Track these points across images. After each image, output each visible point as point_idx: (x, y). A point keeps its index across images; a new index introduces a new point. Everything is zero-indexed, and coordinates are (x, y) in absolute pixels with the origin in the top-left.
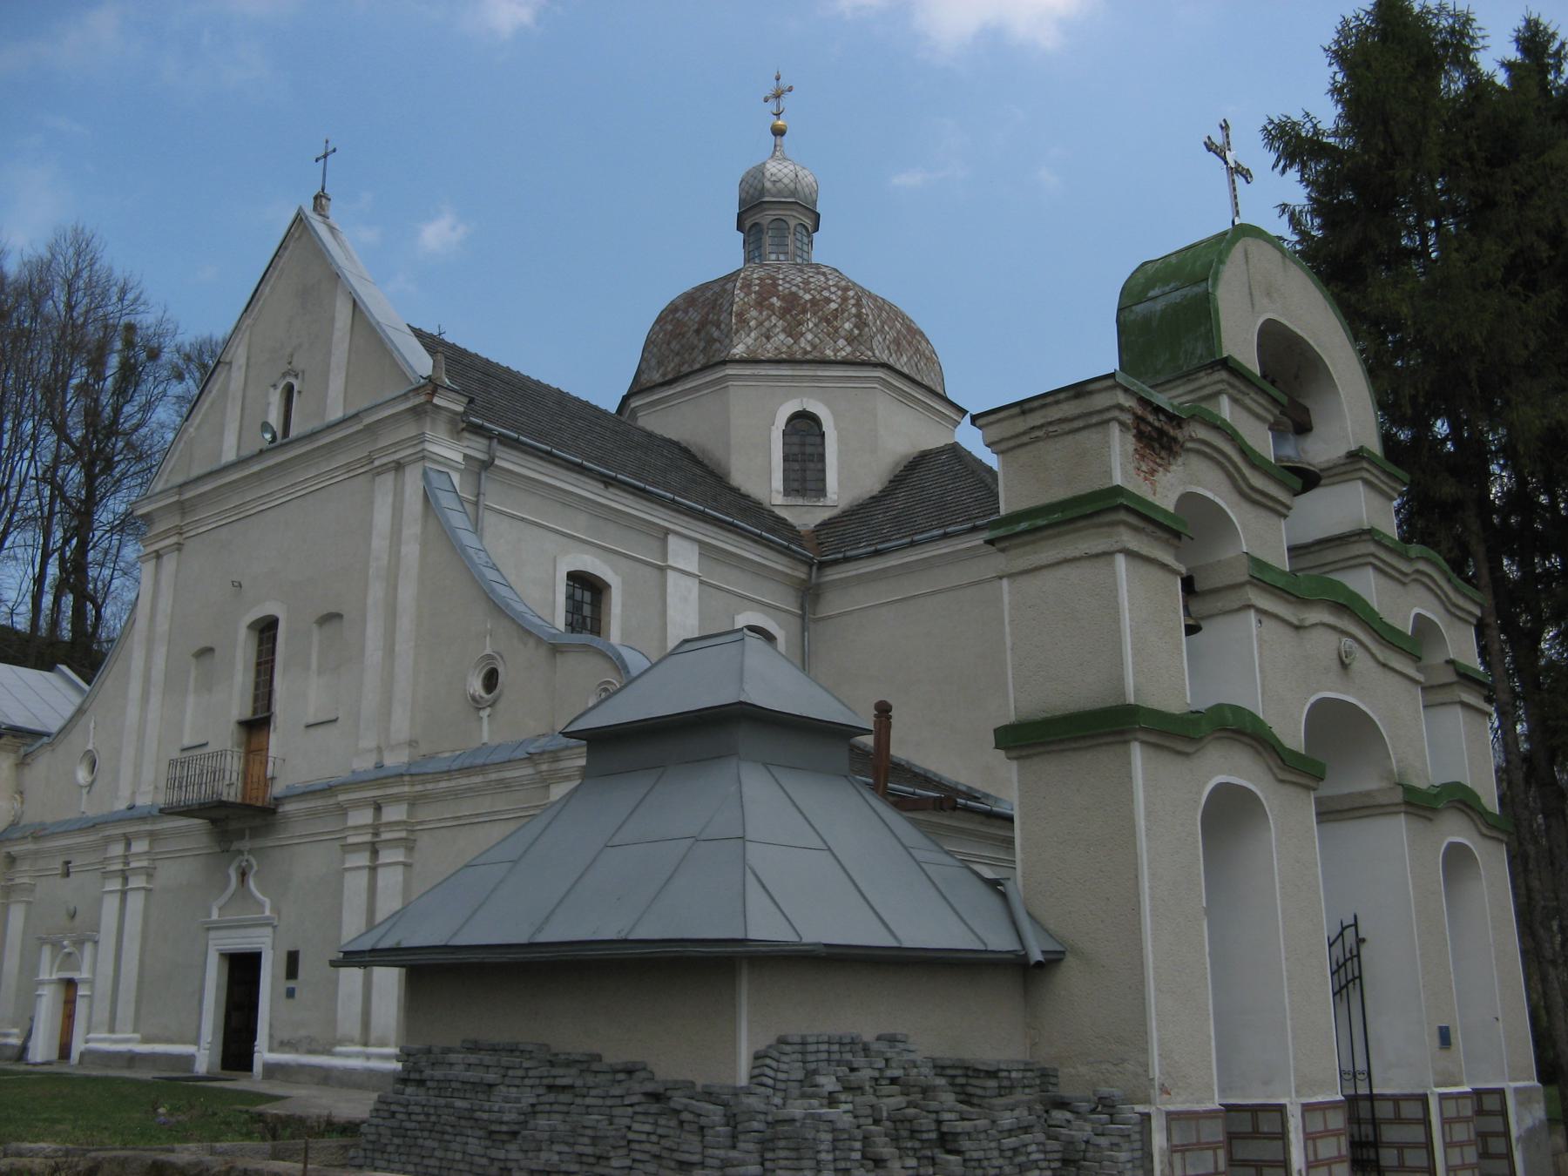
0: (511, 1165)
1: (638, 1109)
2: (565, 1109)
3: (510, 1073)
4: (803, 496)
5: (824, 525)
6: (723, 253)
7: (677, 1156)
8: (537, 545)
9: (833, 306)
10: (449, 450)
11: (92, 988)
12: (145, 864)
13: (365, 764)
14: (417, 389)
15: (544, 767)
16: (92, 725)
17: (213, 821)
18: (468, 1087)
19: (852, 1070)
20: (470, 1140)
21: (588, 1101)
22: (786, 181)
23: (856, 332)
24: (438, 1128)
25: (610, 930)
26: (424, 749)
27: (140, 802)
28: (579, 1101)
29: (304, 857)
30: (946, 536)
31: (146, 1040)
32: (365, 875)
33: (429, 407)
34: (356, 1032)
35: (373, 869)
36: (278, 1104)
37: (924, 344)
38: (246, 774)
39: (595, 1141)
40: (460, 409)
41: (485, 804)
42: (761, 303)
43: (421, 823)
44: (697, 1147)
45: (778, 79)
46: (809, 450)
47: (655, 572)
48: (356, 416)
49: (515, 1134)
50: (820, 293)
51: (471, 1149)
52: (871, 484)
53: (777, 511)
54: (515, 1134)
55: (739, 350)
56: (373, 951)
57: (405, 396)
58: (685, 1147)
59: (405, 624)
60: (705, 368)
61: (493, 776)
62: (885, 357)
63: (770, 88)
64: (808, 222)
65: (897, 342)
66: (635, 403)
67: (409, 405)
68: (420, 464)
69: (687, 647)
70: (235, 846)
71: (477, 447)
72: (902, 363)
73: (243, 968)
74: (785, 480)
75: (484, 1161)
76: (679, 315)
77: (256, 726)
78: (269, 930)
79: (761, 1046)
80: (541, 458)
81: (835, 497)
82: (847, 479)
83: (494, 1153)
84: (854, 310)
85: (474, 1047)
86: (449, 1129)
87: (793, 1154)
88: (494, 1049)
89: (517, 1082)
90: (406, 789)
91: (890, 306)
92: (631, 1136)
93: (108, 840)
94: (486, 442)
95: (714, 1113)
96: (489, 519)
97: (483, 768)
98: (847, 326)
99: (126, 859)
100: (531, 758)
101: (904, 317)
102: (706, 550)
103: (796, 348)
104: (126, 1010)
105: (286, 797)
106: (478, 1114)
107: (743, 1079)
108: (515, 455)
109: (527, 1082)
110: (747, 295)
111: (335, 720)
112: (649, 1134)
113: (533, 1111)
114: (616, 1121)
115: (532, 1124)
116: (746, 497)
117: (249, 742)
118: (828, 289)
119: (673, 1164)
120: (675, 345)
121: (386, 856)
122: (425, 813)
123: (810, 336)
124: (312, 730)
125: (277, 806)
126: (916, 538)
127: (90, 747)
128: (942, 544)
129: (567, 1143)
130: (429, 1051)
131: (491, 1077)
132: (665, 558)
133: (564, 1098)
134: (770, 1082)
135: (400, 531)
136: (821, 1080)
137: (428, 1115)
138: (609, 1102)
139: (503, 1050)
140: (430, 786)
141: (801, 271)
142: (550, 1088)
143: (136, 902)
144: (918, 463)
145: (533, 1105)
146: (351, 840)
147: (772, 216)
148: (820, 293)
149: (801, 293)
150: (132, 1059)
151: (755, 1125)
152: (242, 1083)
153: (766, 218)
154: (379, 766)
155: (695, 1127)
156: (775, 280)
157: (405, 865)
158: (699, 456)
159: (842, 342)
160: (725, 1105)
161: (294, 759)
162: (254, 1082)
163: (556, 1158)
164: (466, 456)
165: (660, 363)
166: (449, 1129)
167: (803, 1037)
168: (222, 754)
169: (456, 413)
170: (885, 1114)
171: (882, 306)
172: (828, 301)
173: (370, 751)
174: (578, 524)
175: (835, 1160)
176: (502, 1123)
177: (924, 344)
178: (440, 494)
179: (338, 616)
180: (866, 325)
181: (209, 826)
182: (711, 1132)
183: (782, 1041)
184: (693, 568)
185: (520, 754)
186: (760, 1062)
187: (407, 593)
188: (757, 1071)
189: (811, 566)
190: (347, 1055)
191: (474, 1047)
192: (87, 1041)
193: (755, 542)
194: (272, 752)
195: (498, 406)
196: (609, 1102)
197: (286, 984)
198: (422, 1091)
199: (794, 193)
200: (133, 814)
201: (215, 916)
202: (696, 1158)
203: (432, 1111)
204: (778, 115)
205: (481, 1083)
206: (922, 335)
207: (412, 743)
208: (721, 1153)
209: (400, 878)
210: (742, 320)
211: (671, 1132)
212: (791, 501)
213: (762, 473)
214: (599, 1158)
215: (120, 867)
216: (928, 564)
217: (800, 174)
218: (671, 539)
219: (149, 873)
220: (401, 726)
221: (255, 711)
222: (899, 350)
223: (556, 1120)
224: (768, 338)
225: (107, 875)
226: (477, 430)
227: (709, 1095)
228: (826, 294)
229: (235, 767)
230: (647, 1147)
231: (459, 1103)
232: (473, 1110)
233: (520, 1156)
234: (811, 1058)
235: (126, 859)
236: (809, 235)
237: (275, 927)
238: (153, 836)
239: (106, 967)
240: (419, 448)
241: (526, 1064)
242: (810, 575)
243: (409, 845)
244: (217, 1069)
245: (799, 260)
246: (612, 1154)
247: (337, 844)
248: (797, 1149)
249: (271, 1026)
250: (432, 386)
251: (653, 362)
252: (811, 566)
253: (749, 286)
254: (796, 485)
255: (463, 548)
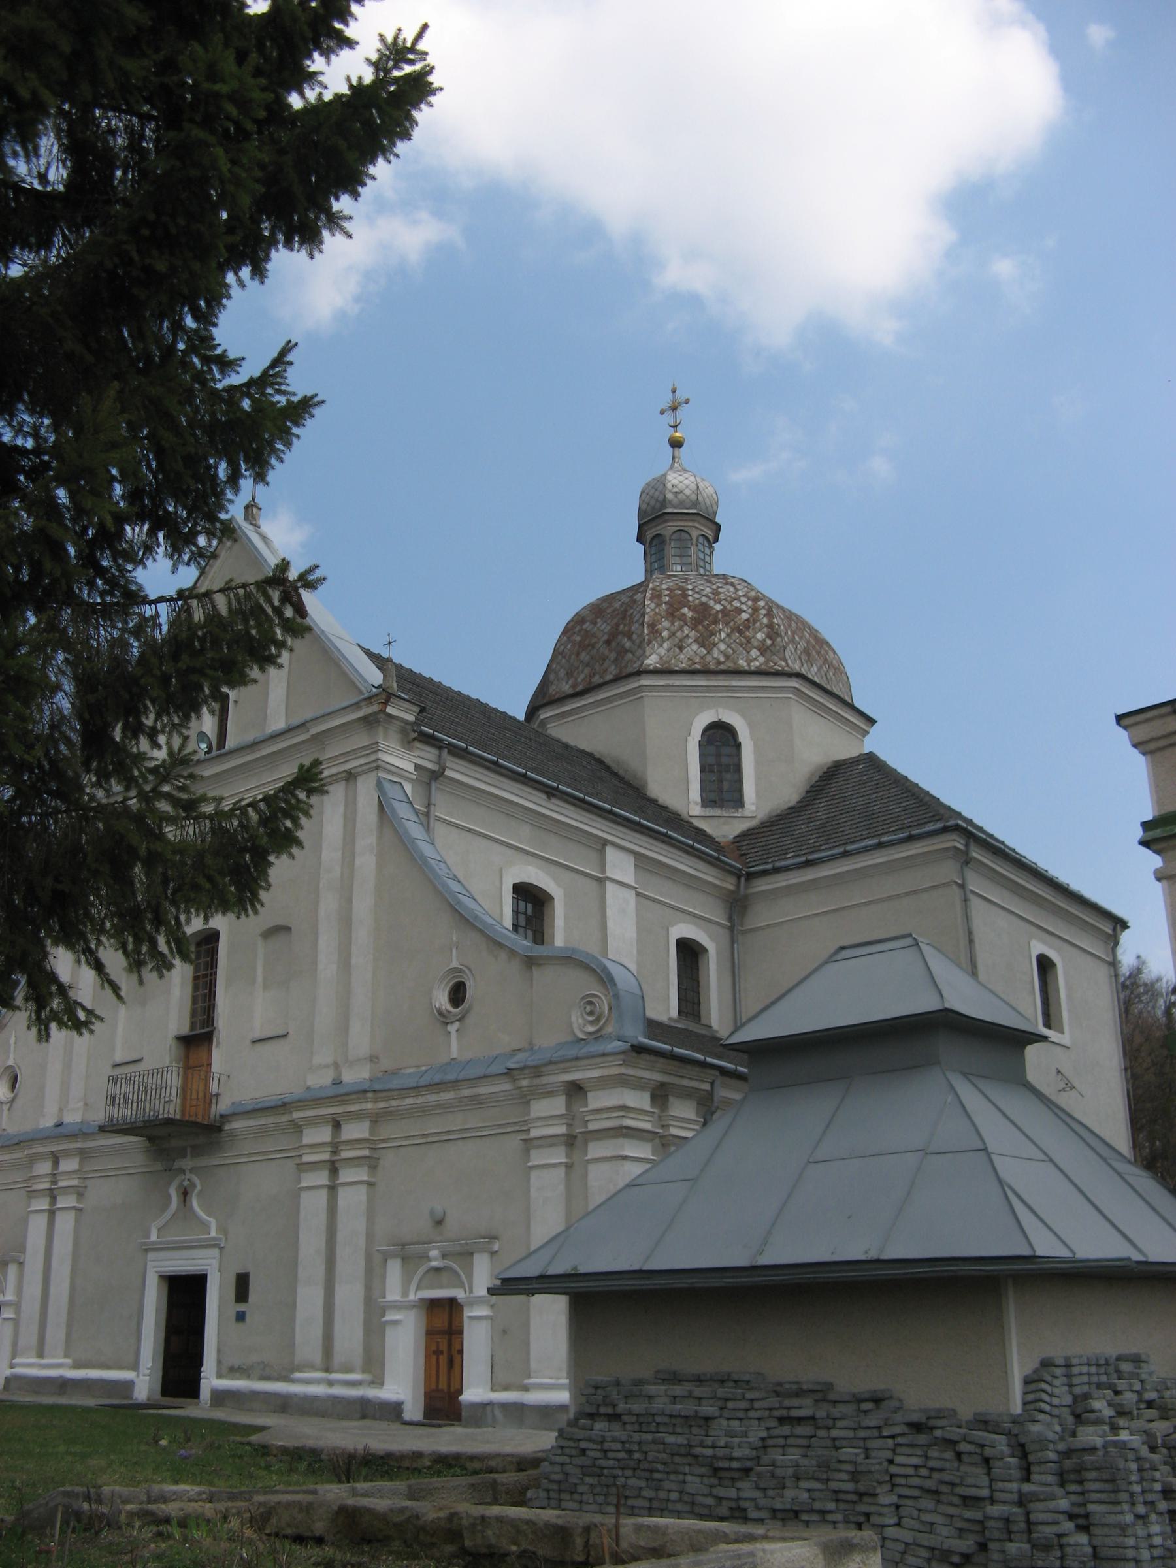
0: (743, 1504)
1: (900, 1440)
2: (804, 1442)
3: (730, 1405)
4: (721, 807)
5: (744, 836)
6: (625, 566)
7: (960, 1490)
8: (489, 853)
9: (745, 616)
10: (401, 759)
11: (18, 1311)
12: (75, 1182)
13: (321, 1080)
14: (369, 698)
15: (525, 1083)
16: (13, 1040)
17: (151, 1139)
18: (678, 1421)
19: (1117, 1393)
20: (689, 1478)
21: (835, 1433)
22: (687, 492)
23: (769, 642)
24: (644, 1465)
25: (854, 1251)
26: (386, 1064)
27: (68, 1119)
28: (822, 1433)
29: (255, 1172)
30: (880, 845)
31: (77, 1366)
32: (323, 1195)
33: (382, 716)
34: (358, 1359)
35: (332, 1189)
36: (264, 1433)
37: (831, 654)
38: (184, 1090)
39: (855, 1476)
40: (411, 718)
41: (456, 1122)
42: (672, 614)
43: (384, 1141)
44: (985, 1481)
45: (674, 391)
46: (724, 760)
47: (593, 885)
48: (303, 725)
49: (747, 1471)
50: (730, 603)
51: (689, 1488)
52: (788, 794)
53: (696, 822)
54: (747, 1471)
55: (652, 661)
56: (542, 1277)
57: (357, 705)
58: (969, 1481)
59: (362, 935)
60: (617, 679)
61: (466, 1092)
62: (797, 667)
63: (666, 400)
64: (710, 534)
65: (806, 652)
66: (544, 714)
67: (361, 714)
68: (374, 774)
69: (844, 954)
70: (176, 1165)
71: (426, 757)
72: (813, 673)
73: (185, 1294)
74: (703, 790)
75: (710, 1501)
76: (586, 626)
77: (197, 1040)
78: (216, 1251)
79: (1028, 1370)
80: (488, 768)
81: (753, 808)
82: (765, 789)
83: (721, 1492)
84: (765, 621)
85: (674, 1378)
86: (660, 1467)
87: (1108, 1487)
88: (699, 1380)
89: (741, 1414)
90: (370, 1106)
91: (796, 616)
92: (893, 1469)
93: (33, 1159)
94: (435, 751)
95: (1001, 1444)
96: (440, 830)
97: (455, 1084)
98: (760, 636)
99: (54, 1178)
100: (509, 1073)
101: (810, 627)
102: (642, 862)
103: (709, 658)
104: (56, 1333)
105: (234, 1114)
106: (698, 1451)
107: (1017, 1408)
108: (461, 765)
109: (752, 1414)
110: (658, 605)
111: (285, 1036)
112: (916, 1467)
113: (764, 1445)
114: (873, 1454)
115: (765, 1459)
116: (664, 808)
117: (187, 1057)
118: (738, 599)
119: (956, 1500)
120: (584, 656)
121: (346, 1175)
122: (388, 1130)
123: (722, 647)
124: (259, 1046)
125: (223, 1123)
126: (849, 848)
127: (11, 1062)
128: (877, 853)
129: (817, 1480)
130: (618, 1383)
131: (708, 1409)
132: (603, 871)
133: (800, 1430)
134: (1047, 1408)
135: (353, 842)
136: (1097, 1405)
137: (630, 1452)
138: (862, 1434)
139: (711, 1379)
140: (394, 1103)
141: (710, 582)
142: (782, 1420)
143: (65, 1223)
144: (834, 772)
145: (763, 1439)
146: (306, 1159)
147: (671, 526)
148: (730, 603)
149: (712, 603)
150: (63, 1385)
151: (1052, 1456)
152: (191, 1411)
153: (668, 529)
154: (337, 1082)
155: (977, 1459)
156: (684, 590)
157: (370, 1184)
158: (614, 766)
159: (754, 653)
160: (1008, 1434)
161: (240, 1074)
162: (202, 1408)
163: (806, 1495)
164: (417, 766)
165: (569, 674)
166: (660, 1467)
167: (1067, 1359)
168: (162, 1071)
169: (406, 722)
170: (1159, 1441)
171: (790, 616)
172: (739, 611)
173: (327, 1066)
174: (522, 835)
175: (1143, 1492)
176: (731, 1459)
177: (831, 654)
178: (396, 805)
179: (287, 929)
180: (779, 635)
181: (147, 1144)
182: (999, 1463)
183: (1046, 1364)
184: (630, 879)
185: (497, 1068)
186: (1033, 1387)
187: (363, 905)
188: (1031, 1397)
189: (739, 877)
190: (307, 1382)
191: (674, 1378)
192: (12, 1366)
193: (687, 852)
194: (215, 1068)
195: (441, 719)
196: (862, 1434)
197: (234, 1308)
198: (616, 1426)
199: (695, 504)
200: (60, 1131)
201: (154, 1237)
202: (985, 1493)
203: (636, 1447)
204: (675, 427)
205: (696, 1416)
206: (827, 644)
207: (373, 1059)
208: (1014, 1486)
209: (364, 1198)
210: (655, 631)
211: (947, 1465)
212: (710, 812)
213: (680, 784)
214: (861, 1495)
215: (47, 1186)
216: (862, 873)
217: (701, 485)
218: (609, 850)
219: (80, 1193)
220: (361, 1040)
221: (193, 1026)
222: (810, 661)
223: (793, 1455)
224: (681, 649)
225: (32, 1194)
226: (428, 740)
227: (983, 1422)
228: (736, 604)
229: (175, 1083)
230: (915, 1481)
231: (670, 1439)
232: (691, 1446)
233: (757, 1494)
234: (1076, 1381)
235: (54, 1178)
236: (711, 547)
237: (221, 1248)
238: (83, 1154)
239: (33, 1289)
240: (373, 757)
241: (749, 1395)
242: (738, 886)
243: (372, 1163)
244: (157, 1396)
245: (702, 571)
246: (878, 1490)
247: (291, 1164)
248: (1113, 1481)
249: (219, 1351)
250: (385, 695)
251: (562, 673)
252: (739, 877)
253: (659, 596)
254: (713, 796)
255: (424, 859)
